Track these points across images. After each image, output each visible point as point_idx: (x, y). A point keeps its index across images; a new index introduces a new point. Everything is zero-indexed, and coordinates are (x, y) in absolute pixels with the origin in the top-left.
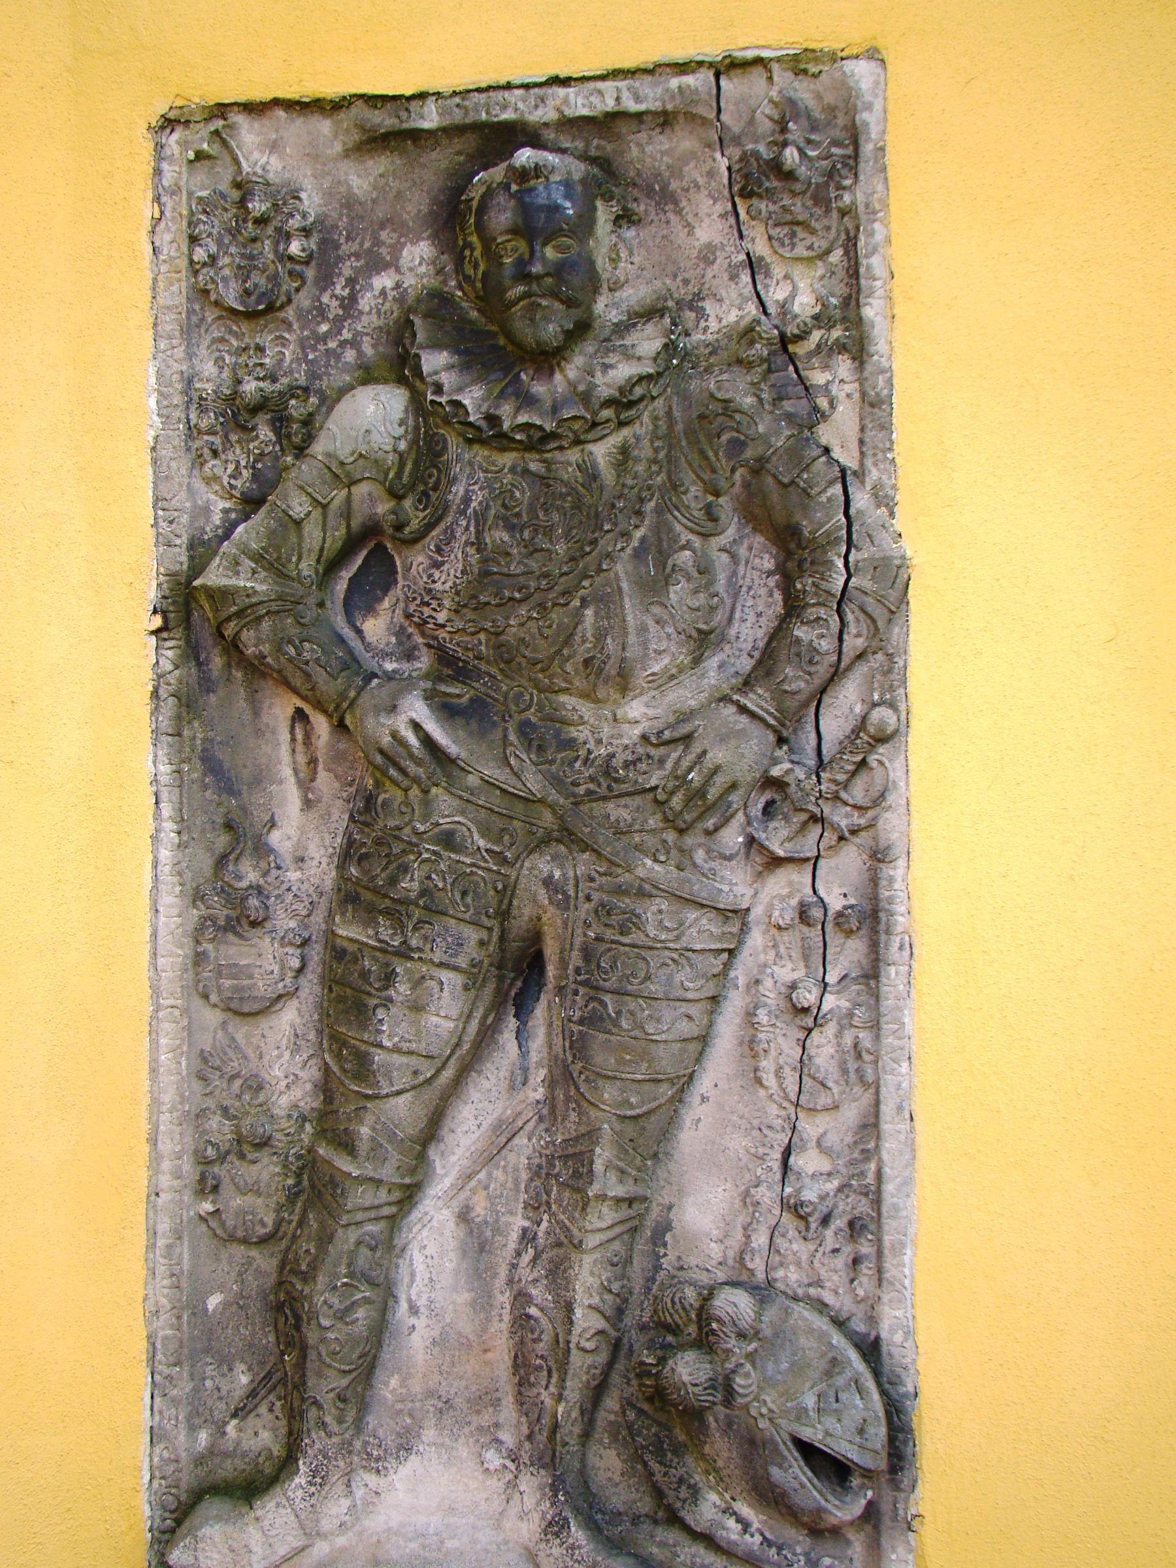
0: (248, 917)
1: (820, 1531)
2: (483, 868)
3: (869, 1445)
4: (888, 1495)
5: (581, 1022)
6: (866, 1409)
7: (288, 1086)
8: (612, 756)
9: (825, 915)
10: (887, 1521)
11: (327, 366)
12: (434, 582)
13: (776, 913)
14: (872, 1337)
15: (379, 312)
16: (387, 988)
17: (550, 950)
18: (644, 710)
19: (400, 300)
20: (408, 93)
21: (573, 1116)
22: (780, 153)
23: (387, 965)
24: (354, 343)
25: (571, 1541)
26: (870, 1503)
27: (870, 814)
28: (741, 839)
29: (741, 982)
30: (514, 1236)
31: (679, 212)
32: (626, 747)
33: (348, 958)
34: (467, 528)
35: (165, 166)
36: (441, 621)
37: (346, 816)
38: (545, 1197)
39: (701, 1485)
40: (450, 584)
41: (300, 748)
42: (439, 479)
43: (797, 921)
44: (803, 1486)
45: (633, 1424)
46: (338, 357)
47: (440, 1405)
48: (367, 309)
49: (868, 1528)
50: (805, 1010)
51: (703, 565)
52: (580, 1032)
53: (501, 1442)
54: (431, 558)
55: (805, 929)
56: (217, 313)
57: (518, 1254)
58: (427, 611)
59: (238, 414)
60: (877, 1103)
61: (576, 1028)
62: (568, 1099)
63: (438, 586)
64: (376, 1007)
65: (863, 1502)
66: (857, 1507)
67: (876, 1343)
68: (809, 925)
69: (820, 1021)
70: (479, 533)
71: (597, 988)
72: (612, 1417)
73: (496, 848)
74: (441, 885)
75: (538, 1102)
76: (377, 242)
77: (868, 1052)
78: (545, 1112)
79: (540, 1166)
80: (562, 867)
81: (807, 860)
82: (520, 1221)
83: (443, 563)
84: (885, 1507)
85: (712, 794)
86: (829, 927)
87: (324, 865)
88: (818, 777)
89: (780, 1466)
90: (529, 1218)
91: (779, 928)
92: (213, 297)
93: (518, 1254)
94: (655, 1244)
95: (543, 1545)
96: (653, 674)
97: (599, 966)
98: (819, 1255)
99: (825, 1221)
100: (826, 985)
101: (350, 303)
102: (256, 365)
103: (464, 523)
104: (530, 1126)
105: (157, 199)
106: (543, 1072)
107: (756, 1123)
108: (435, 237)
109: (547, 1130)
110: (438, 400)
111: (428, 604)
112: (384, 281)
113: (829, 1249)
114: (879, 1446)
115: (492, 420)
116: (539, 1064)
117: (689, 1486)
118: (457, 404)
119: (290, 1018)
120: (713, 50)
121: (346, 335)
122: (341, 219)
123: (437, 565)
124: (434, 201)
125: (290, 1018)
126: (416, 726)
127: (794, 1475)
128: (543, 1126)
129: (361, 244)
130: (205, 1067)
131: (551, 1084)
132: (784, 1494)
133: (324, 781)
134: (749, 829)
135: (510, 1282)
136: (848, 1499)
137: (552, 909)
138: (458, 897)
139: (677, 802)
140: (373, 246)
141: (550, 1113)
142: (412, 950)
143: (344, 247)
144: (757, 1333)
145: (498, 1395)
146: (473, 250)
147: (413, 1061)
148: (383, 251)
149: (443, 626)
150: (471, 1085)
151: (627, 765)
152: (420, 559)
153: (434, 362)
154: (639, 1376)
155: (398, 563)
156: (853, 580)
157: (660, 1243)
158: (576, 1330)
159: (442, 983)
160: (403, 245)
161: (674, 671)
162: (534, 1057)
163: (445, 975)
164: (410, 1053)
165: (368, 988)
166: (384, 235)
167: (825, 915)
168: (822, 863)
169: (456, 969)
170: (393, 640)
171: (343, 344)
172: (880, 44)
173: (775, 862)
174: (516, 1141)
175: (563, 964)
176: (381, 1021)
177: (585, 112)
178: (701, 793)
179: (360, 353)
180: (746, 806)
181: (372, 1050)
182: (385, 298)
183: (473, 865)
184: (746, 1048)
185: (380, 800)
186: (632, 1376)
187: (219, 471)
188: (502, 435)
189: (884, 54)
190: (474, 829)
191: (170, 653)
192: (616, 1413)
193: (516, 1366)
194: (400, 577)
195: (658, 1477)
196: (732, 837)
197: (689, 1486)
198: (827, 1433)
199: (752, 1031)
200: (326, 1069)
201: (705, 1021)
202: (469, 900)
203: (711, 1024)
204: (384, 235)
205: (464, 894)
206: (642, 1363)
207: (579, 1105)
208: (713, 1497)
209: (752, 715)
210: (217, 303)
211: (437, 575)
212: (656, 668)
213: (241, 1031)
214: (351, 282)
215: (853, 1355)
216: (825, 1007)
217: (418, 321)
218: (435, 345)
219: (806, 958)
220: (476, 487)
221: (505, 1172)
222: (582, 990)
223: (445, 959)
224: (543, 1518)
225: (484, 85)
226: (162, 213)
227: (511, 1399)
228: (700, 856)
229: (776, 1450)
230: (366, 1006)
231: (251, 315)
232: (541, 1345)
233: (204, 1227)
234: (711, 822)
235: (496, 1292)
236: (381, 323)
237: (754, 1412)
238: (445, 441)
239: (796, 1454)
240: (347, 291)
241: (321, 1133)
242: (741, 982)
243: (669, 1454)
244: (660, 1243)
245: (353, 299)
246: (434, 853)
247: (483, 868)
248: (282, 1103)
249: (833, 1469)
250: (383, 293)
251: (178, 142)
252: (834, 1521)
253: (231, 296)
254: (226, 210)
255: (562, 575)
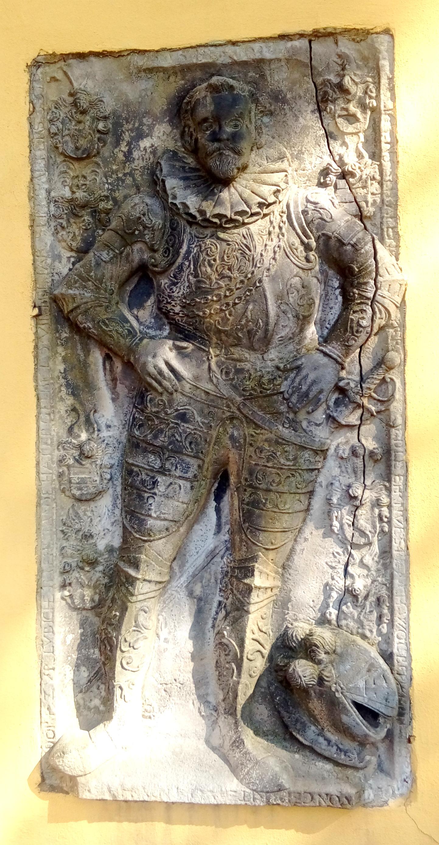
0: (84, 454)
1: (363, 742)
2: (200, 431)
3: (390, 705)
4: (397, 726)
5: (248, 504)
6: (389, 688)
7: (104, 534)
8: (262, 377)
9: (365, 452)
10: (396, 739)
11: (118, 185)
12: (173, 292)
13: (341, 452)
14: (389, 652)
15: (143, 159)
16: (153, 488)
17: (233, 469)
18: (277, 354)
19: (154, 152)
20: (156, 49)
21: (244, 549)
22: (342, 80)
23: (153, 477)
24: (131, 174)
25: (245, 750)
26: (389, 730)
27: (386, 404)
28: (324, 416)
29: (324, 484)
30: (215, 605)
31: (291, 109)
32: (269, 372)
33: (134, 474)
34: (189, 266)
35: (36, 85)
36: (176, 311)
37: (131, 406)
38: (230, 587)
39: (306, 722)
40: (181, 293)
41: (108, 372)
42: (175, 241)
43: (351, 454)
44: (357, 724)
45: (273, 693)
46: (123, 181)
47: (179, 685)
48: (137, 157)
49: (387, 741)
50: (355, 498)
51: (305, 284)
52: (248, 509)
53: (210, 703)
54: (171, 280)
55: (354, 458)
56: (62, 158)
57: (217, 613)
58: (169, 307)
59: (74, 208)
60: (391, 541)
61: (246, 507)
62: (241, 540)
63: (175, 294)
64: (148, 497)
65: (386, 730)
66: (383, 734)
67: (391, 655)
68: (357, 457)
69: (363, 502)
70: (195, 269)
71: (257, 488)
72: (263, 690)
73: (206, 421)
74: (179, 439)
75: (226, 541)
76: (141, 124)
77: (386, 517)
78: (229, 545)
79: (227, 572)
80: (238, 430)
81: (356, 425)
82: (218, 598)
83: (177, 283)
84: (396, 732)
85: (311, 396)
86: (366, 458)
87: (121, 429)
88: (361, 387)
89: (347, 715)
90: (222, 596)
91: (342, 458)
92: (61, 150)
93: (217, 613)
94: (283, 608)
95: (231, 752)
96: (281, 337)
97: (256, 477)
98: (363, 614)
99: (366, 597)
100: (365, 485)
101: (128, 155)
102: (83, 185)
103: (187, 263)
104: (222, 553)
105: (31, 102)
106: (228, 527)
107: (331, 550)
108: (170, 121)
109: (231, 555)
110: (174, 202)
111: (170, 303)
112: (145, 143)
113: (368, 610)
114: (395, 706)
115: (202, 212)
116: (226, 523)
117: (301, 723)
118: (184, 204)
119: (105, 503)
120: (308, 28)
121: (127, 171)
122: (123, 112)
123: (175, 284)
124: (168, 104)
125: (105, 503)
126: (167, 364)
127: (355, 718)
128: (228, 552)
129: (134, 125)
130: (65, 530)
131: (231, 533)
132: (348, 728)
133: (121, 389)
134: (328, 412)
135: (213, 626)
136: (378, 729)
137: (233, 450)
138: (188, 445)
139: (294, 399)
140: (140, 125)
141: (231, 547)
142: (166, 470)
143: (125, 126)
144: (334, 651)
145: (207, 680)
146: (189, 127)
147: (166, 523)
148: (145, 128)
149: (178, 314)
150: (193, 533)
151: (270, 381)
152: (166, 281)
153: (171, 183)
154: (276, 671)
155: (155, 283)
156: (379, 291)
157: (285, 608)
158: (246, 650)
159: (180, 486)
160: (155, 125)
161: (291, 335)
162: (223, 520)
163: (181, 482)
164: (165, 520)
165: (144, 489)
166: (145, 120)
167: (365, 452)
168: (362, 428)
169: (186, 479)
170: (153, 320)
171: (125, 175)
172: (391, 26)
173: (340, 426)
174: (215, 559)
175: (238, 476)
176: (151, 504)
177: (245, 59)
178: (306, 394)
179: (134, 180)
180: (327, 401)
181: (146, 518)
182: (146, 152)
183: (195, 429)
184: (326, 514)
185: (148, 398)
186: (272, 670)
187: (65, 237)
188: (208, 220)
189: (393, 32)
190: (195, 412)
191: (43, 327)
192: (265, 688)
193: (217, 667)
194: (156, 290)
195: (286, 719)
196: (320, 415)
197: (301, 723)
198: (370, 699)
199: (330, 507)
200: (124, 527)
201: (307, 502)
202: (193, 446)
203: (310, 504)
204: (145, 120)
205: (191, 443)
206: (278, 665)
207: (247, 543)
208: (313, 728)
209: (330, 356)
210: (62, 154)
211: (174, 289)
212: (283, 334)
213: (82, 508)
214: (129, 144)
215: (381, 661)
216: (365, 496)
217: (162, 163)
218: (171, 174)
219: (355, 472)
220: (193, 246)
221: (210, 574)
222: (249, 489)
223: (181, 474)
224: (231, 739)
225: (194, 45)
226: (34, 108)
227: (214, 682)
228: (304, 424)
229: (345, 707)
230: (143, 497)
231: (79, 159)
232: (230, 657)
233: (64, 602)
234: (311, 408)
235: (207, 631)
236: (145, 163)
237: (333, 689)
238: (178, 223)
239: (355, 709)
240: (127, 148)
241: (121, 558)
242: (324, 484)
243: (291, 708)
244: (285, 608)
245: (130, 152)
246: (177, 424)
247: (200, 431)
248: (101, 545)
249: (370, 715)
250: (145, 149)
251: (42, 73)
252: (373, 740)
253: (70, 149)
254: (66, 107)
255: (237, 289)
